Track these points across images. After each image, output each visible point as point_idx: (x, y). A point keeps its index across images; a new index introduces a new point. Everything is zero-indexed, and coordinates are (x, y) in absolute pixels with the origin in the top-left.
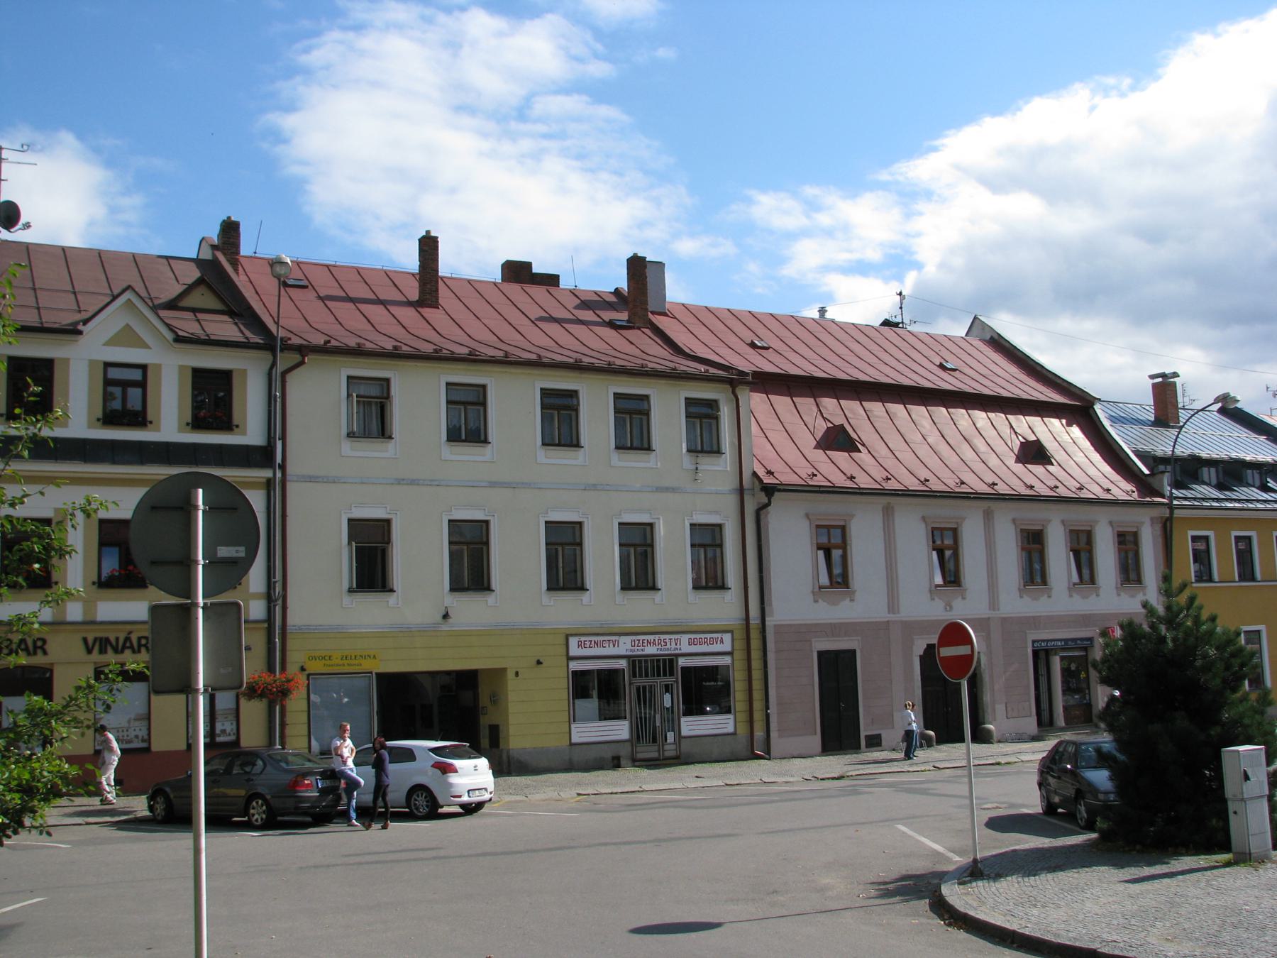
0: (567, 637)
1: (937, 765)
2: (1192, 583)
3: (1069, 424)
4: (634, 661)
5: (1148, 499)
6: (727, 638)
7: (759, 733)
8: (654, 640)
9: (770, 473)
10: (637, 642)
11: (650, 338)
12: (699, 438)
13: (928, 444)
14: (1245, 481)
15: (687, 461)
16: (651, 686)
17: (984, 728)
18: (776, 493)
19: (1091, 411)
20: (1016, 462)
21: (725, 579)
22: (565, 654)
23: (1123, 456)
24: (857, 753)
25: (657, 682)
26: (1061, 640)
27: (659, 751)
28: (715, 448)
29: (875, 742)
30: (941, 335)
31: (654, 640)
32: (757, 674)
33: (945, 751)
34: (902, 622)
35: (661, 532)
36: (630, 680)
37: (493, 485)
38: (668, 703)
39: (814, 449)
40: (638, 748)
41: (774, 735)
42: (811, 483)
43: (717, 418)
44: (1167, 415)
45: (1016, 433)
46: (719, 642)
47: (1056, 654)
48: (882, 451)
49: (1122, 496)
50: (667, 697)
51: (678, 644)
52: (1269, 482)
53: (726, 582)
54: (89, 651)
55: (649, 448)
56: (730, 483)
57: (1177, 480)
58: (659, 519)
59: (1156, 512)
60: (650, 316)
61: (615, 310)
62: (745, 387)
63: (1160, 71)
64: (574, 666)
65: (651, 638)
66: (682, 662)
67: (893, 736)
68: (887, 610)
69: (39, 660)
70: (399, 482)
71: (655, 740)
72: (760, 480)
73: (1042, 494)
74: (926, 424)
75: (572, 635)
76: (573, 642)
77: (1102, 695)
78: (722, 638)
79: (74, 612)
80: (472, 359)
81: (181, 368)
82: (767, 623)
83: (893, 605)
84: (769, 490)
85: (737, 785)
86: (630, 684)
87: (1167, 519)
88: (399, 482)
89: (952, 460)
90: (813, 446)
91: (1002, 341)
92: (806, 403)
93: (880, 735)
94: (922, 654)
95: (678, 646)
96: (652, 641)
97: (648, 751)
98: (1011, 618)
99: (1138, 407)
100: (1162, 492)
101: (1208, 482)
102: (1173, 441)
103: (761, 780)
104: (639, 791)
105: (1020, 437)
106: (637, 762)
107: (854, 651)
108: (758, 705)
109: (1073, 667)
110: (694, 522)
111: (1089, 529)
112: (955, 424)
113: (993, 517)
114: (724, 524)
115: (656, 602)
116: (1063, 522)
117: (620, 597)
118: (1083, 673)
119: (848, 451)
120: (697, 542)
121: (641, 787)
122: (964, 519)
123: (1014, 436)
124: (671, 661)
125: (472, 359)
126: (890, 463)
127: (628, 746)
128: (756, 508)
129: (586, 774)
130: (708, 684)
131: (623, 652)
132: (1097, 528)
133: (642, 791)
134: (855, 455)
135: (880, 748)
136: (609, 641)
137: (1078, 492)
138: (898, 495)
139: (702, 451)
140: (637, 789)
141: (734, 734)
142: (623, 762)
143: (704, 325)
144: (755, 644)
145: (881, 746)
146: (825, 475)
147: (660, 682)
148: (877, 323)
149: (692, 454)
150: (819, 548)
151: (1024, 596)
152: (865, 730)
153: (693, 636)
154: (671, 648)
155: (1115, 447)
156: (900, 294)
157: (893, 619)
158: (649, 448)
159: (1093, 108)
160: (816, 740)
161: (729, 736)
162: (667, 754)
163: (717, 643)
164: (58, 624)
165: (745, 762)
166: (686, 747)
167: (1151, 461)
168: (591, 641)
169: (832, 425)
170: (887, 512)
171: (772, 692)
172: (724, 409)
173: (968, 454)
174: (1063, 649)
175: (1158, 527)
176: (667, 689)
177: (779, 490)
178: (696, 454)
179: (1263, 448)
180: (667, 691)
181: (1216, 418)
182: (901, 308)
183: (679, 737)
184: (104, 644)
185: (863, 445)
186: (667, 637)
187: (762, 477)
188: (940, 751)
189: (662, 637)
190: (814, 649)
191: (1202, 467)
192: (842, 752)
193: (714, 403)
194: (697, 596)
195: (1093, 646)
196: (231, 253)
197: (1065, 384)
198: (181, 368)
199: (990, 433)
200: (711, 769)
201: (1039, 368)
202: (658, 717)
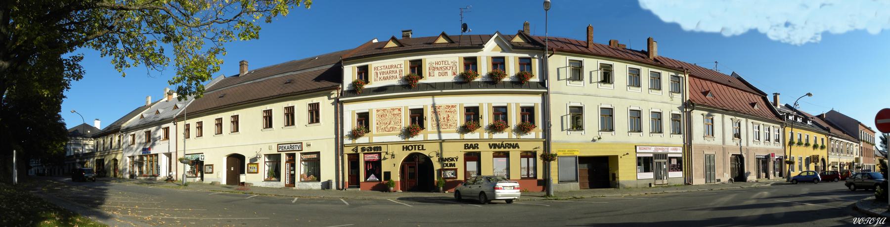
37: (614, 97)
38: (665, 167)
50: (665, 166)
54: (491, 148)
64: (638, 155)
65: (660, 147)
69: (476, 150)
76: (638, 148)
77: (812, 167)
124: (666, 155)
131: (652, 152)
154: (665, 151)
159: (698, 24)
176: (665, 163)
184: (495, 146)
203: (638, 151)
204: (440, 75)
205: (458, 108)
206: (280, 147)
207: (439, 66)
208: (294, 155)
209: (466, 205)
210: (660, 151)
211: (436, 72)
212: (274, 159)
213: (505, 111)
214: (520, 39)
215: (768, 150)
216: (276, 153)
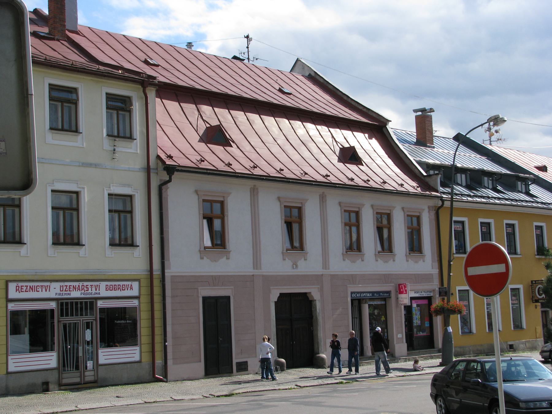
0: (7, 282)
1: (298, 384)
2: (454, 254)
3: (370, 138)
4: (62, 304)
5: (428, 193)
6: (135, 285)
7: (159, 361)
8: (79, 286)
9: (170, 157)
10: (65, 288)
11: (68, 48)
12: (116, 126)
13: (278, 144)
14: (483, 185)
15: (107, 144)
16: (76, 323)
17: (319, 357)
18: (176, 173)
19: (384, 130)
20: (338, 162)
21: (134, 239)
22: (4, 296)
23: (407, 161)
24: (230, 376)
25: (80, 320)
26: (369, 292)
27: (81, 377)
28: (128, 135)
29: (243, 367)
30: (275, 70)
31: (79, 286)
32: (158, 315)
33: (294, 374)
34: (263, 276)
35: (85, 198)
36: (58, 318)
38: (88, 337)
39: (198, 142)
40: (64, 374)
41: (170, 362)
42: (201, 167)
43: (130, 112)
44: (425, 138)
45: (336, 141)
46: (129, 289)
47: (366, 303)
48: (247, 148)
49: (411, 190)
50: (88, 333)
52: (498, 187)
53: (134, 241)
55: (76, 131)
56: (139, 163)
57: (441, 181)
58: (84, 188)
59: (431, 202)
60: (67, 32)
61: (37, 25)
62: (152, 88)
64: (12, 306)
65: (76, 284)
66: (100, 304)
67: (254, 364)
68: (252, 266)
71: (77, 368)
72: (163, 162)
73: (360, 185)
74: (275, 130)
75: (11, 281)
76: (12, 286)
78: (131, 285)
82: (166, 274)
83: (257, 263)
84: (171, 170)
85: (154, 402)
86: (59, 322)
87: (439, 208)
89: (296, 157)
90: (198, 141)
91: (318, 77)
92: (190, 108)
93: (247, 362)
94: (276, 300)
95: (98, 291)
96: (77, 287)
97: (72, 377)
98: (337, 275)
99: (404, 132)
100: (436, 188)
101: (461, 184)
102: (455, 149)
103: (171, 398)
104: (75, 410)
105: (339, 144)
106: (63, 386)
107: (228, 298)
108: (158, 339)
109: (376, 312)
110: (112, 192)
111: (389, 212)
112: (295, 132)
113: (326, 201)
114: (135, 195)
115: (80, 256)
116: (372, 206)
117: (52, 251)
118: (383, 317)
119: (223, 145)
120: (114, 208)
121: (76, 407)
122: (307, 200)
123: (335, 143)
124: (92, 303)
126: (253, 156)
127: (56, 373)
128: (159, 183)
129: (20, 398)
130: (119, 322)
132: (394, 211)
133: (79, 410)
134: (228, 148)
135: (246, 372)
136: (42, 286)
137: (382, 185)
138: (263, 179)
139: (118, 136)
140: (74, 408)
141: (140, 362)
142: (51, 386)
143: (107, 44)
144: (157, 290)
145: (247, 370)
146: (209, 161)
147: (83, 320)
148: (230, 57)
149: (110, 138)
150: (204, 218)
151: (346, 259)
152: (236, 359)
153: (109, 283)
154: (92, 293)
155: (401, 155)
156: (247, 37)
157: (256, 274)
158: (76, 131)
160: (201, 366)
161: (136, 364)
162: (87, 379)
163: (127, 290)
165: (149, 384)
166: (102, 373)
167: (425, 167)
168: (27, 286)
169: (210, 126)
170: (253, 192)
171: (169, 329)
172: (136, 104)
173: (306, 154)
174: (371, 299)
175: (433, 213)
176: (88, 325)
177: (178, 171)
178: (114, 138)
179: (486, 164)
180: (88, 327)
181: (452, 142)
182: (248, 47)
183: (97, 365)
185: (233, 142)
186: (89, 284)
187: (164, 160)
188: (290, 374)
189: (85, 284)
190: (200, 296)
191: (457, 173)
192: (221, 375)
193: (127, 99)
194: (113, 252)
195: (390, 297)
197: (365, 110)
199: (318, 139)
200: (123, 390)
201: (345, 98)
202: (80, 348)
203: (13, 294)
210: (75, 294)
213: (357, 301)
214: (35, 16)
215: (386, 278)
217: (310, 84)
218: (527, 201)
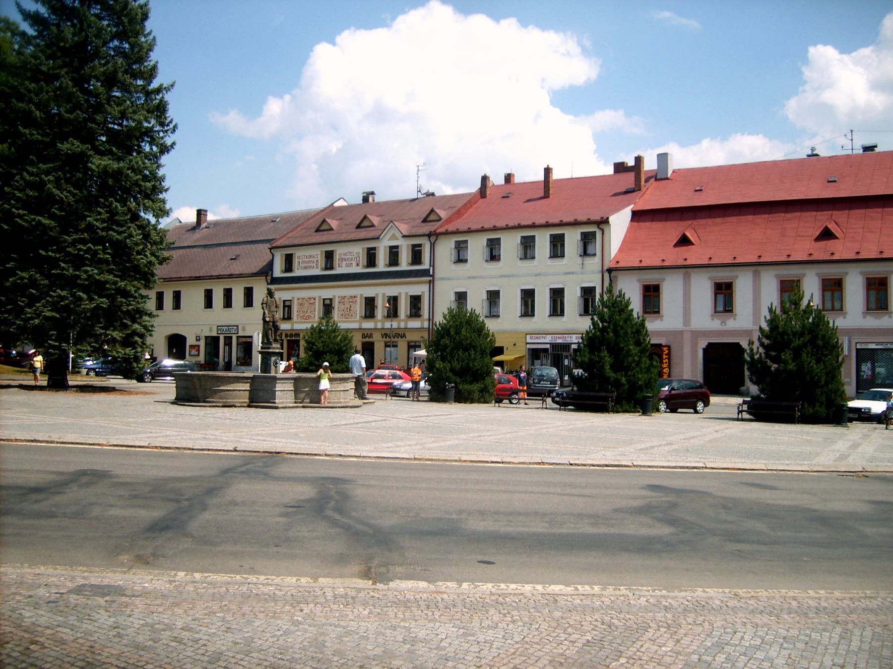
15: (579, 260)
37: (501, 276)
51: (312, 265)
63: (596, 155)
64: (529, 346)
65: (560, 336)
69: (371, 340)
70: (469, 278)
76: (528, 336)
79: (379, 326)
80: (495, 229)
81: (408, 245)
88: (469, 278)
117: (548, 319)
125: (495, 229)
164: (376, 329)
184: (386, 335)
196: (32, 633)
198: (408, 245)
204: (347, 266)
205: (358, 299)
206: (220, 330)
207: (346, 257)
208: (231, 338)
209: (710, 221)
211: (344, 263)
212: (212, 342)
216: (216, 335)
217: (843, 457)
218: (655, 497)
